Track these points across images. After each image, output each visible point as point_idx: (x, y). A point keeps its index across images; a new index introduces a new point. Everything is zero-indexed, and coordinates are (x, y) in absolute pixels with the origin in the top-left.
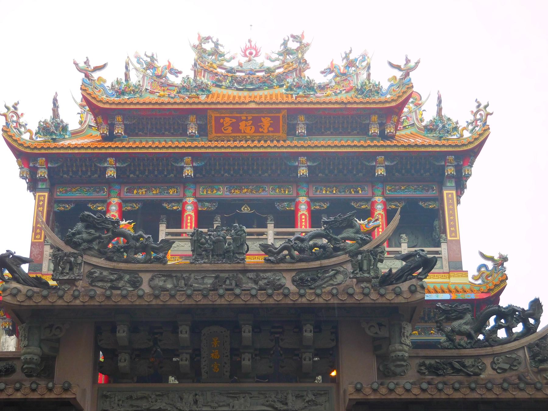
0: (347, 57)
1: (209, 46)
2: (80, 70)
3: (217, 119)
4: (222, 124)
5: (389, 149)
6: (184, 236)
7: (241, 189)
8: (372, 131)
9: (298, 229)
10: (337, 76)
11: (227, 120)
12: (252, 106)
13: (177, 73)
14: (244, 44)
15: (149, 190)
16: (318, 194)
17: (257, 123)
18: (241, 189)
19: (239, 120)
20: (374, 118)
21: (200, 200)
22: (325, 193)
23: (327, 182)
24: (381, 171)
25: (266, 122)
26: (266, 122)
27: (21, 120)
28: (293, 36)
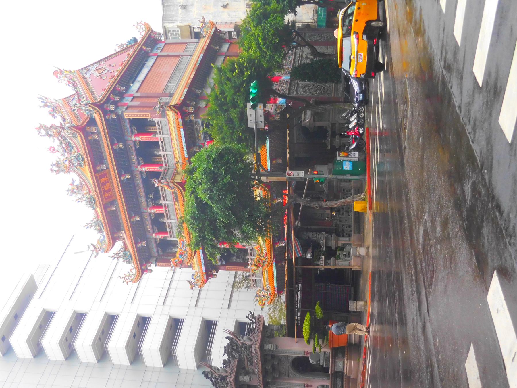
1: (55, 168)
2: (97, 254)
4: (108, 197)
5: (110, 145)
6: (167, 212)
8: (115, 209)
10: (55, 112)
11: (105, 195)
13: (73, 181)
15: (147, 225)
16: (136, 163)
17: (103, 184)
19: (104, 191)
20: (90, 138)
22: (134, 160)
23: (129, 160)
25: (102, 180)
26: (102, 180)
27: (127, 274)
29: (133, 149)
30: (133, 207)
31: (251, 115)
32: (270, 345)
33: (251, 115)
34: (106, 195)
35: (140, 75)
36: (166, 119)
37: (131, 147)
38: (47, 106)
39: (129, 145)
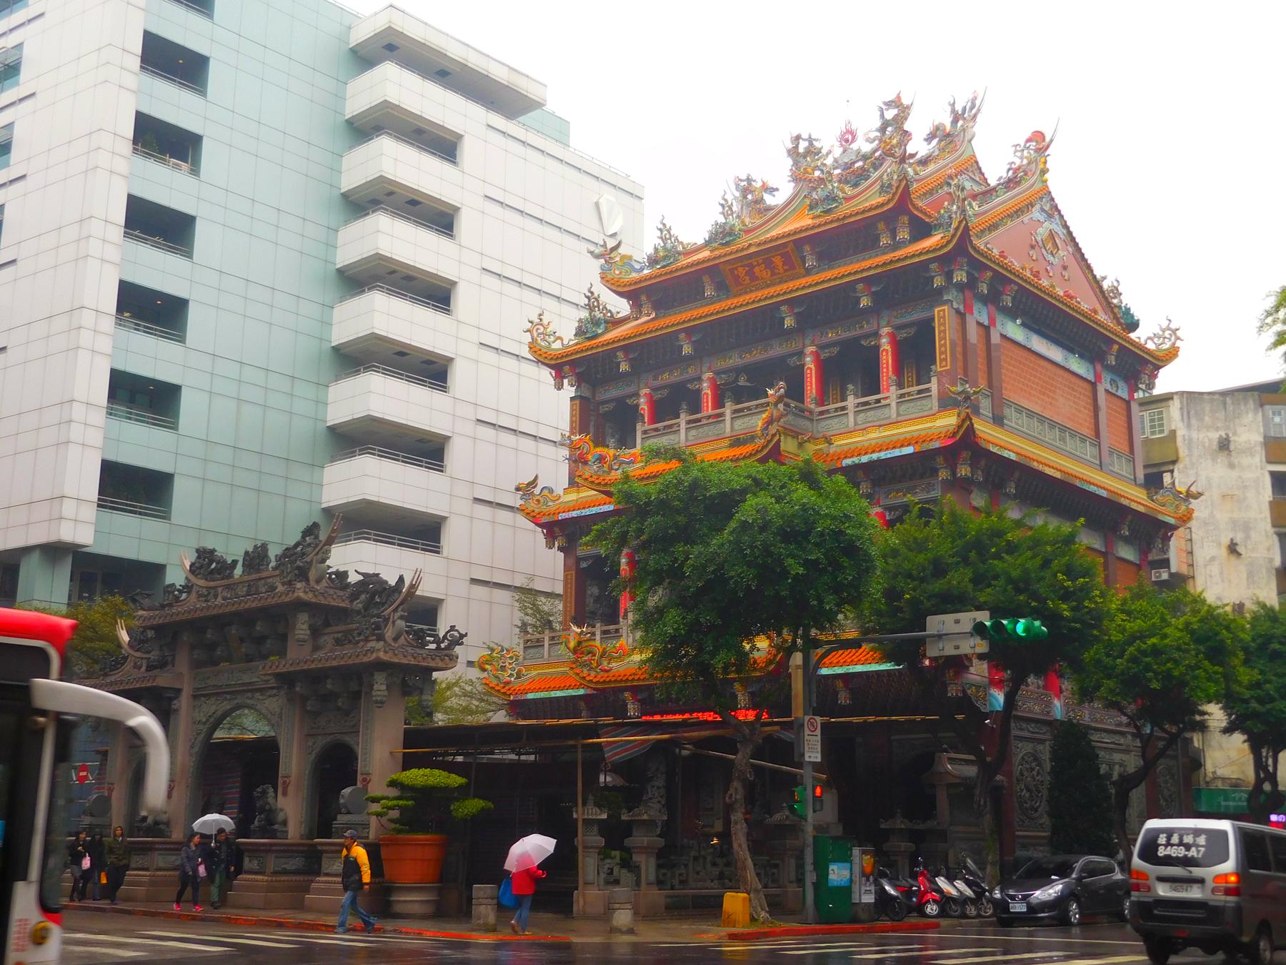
0: (953, 111)
1: (803, 146)
2: (597, 257)
3: (793, 267)
5: (865, 274)
6: (704, 422)
7: (750, 353)
9: (704, 414)
10: (940, 141)
11: (740, 269)
12: (753, 250)
13: (772, 190)
14: (838, 128)
15: (671, 372)
16: (824, 340)
17: (769, 264)
18: (750, 353)
19: (751, 267)
20: (881, 226)
21: (717, 373)
22: (734, 360)
24: (865, 302)
25: (778, 261)
26: (778, 261)
28: (886, 104)
29: (859, 332)
30: (713, 337)
31: (957, 622)
32: (384, 687)
33: (957, 622)
34: (741, 271)
35: (1045, 341)
36: (936, 408)
37: (862, 327)
38: (955, 121)
39: (868, 323)
